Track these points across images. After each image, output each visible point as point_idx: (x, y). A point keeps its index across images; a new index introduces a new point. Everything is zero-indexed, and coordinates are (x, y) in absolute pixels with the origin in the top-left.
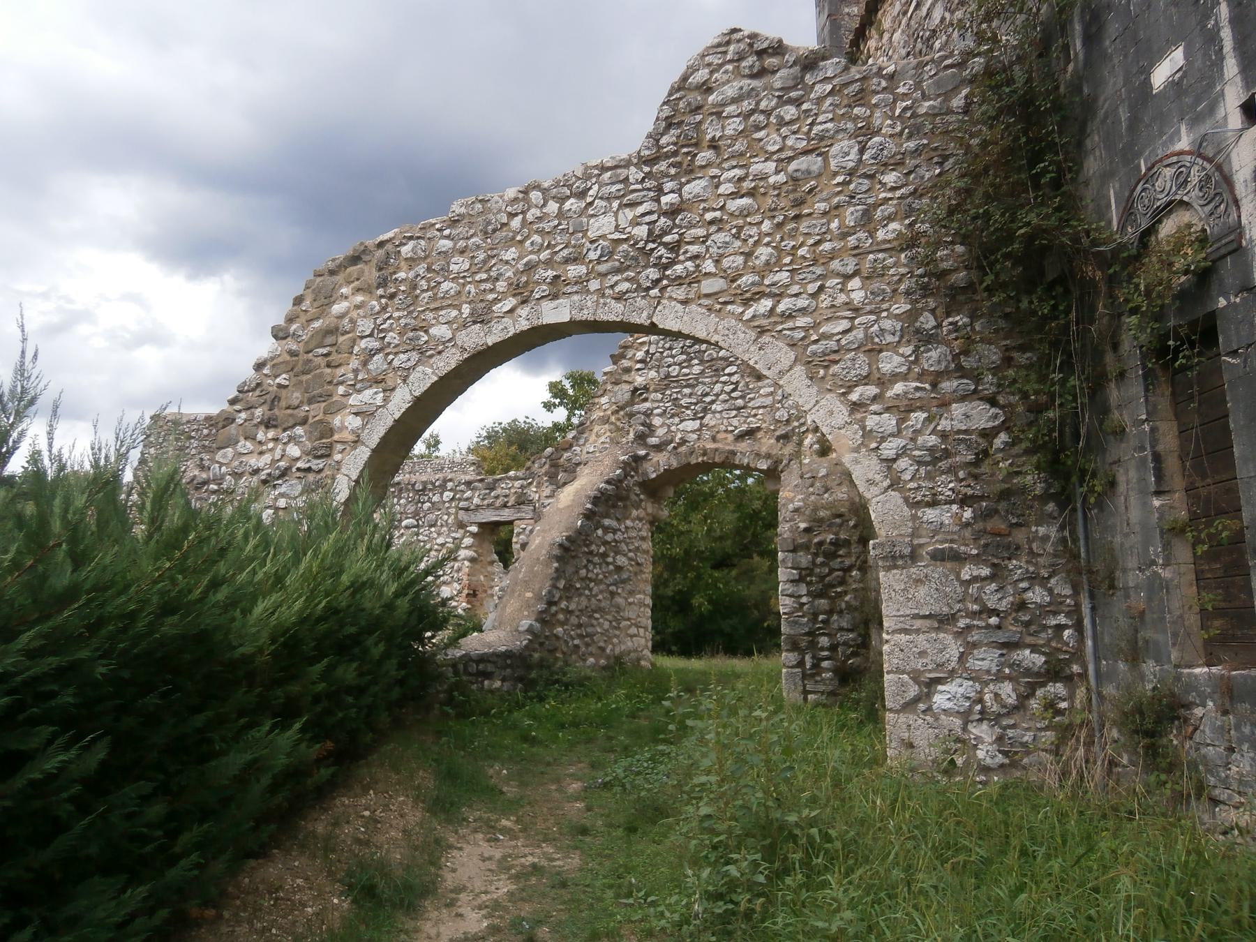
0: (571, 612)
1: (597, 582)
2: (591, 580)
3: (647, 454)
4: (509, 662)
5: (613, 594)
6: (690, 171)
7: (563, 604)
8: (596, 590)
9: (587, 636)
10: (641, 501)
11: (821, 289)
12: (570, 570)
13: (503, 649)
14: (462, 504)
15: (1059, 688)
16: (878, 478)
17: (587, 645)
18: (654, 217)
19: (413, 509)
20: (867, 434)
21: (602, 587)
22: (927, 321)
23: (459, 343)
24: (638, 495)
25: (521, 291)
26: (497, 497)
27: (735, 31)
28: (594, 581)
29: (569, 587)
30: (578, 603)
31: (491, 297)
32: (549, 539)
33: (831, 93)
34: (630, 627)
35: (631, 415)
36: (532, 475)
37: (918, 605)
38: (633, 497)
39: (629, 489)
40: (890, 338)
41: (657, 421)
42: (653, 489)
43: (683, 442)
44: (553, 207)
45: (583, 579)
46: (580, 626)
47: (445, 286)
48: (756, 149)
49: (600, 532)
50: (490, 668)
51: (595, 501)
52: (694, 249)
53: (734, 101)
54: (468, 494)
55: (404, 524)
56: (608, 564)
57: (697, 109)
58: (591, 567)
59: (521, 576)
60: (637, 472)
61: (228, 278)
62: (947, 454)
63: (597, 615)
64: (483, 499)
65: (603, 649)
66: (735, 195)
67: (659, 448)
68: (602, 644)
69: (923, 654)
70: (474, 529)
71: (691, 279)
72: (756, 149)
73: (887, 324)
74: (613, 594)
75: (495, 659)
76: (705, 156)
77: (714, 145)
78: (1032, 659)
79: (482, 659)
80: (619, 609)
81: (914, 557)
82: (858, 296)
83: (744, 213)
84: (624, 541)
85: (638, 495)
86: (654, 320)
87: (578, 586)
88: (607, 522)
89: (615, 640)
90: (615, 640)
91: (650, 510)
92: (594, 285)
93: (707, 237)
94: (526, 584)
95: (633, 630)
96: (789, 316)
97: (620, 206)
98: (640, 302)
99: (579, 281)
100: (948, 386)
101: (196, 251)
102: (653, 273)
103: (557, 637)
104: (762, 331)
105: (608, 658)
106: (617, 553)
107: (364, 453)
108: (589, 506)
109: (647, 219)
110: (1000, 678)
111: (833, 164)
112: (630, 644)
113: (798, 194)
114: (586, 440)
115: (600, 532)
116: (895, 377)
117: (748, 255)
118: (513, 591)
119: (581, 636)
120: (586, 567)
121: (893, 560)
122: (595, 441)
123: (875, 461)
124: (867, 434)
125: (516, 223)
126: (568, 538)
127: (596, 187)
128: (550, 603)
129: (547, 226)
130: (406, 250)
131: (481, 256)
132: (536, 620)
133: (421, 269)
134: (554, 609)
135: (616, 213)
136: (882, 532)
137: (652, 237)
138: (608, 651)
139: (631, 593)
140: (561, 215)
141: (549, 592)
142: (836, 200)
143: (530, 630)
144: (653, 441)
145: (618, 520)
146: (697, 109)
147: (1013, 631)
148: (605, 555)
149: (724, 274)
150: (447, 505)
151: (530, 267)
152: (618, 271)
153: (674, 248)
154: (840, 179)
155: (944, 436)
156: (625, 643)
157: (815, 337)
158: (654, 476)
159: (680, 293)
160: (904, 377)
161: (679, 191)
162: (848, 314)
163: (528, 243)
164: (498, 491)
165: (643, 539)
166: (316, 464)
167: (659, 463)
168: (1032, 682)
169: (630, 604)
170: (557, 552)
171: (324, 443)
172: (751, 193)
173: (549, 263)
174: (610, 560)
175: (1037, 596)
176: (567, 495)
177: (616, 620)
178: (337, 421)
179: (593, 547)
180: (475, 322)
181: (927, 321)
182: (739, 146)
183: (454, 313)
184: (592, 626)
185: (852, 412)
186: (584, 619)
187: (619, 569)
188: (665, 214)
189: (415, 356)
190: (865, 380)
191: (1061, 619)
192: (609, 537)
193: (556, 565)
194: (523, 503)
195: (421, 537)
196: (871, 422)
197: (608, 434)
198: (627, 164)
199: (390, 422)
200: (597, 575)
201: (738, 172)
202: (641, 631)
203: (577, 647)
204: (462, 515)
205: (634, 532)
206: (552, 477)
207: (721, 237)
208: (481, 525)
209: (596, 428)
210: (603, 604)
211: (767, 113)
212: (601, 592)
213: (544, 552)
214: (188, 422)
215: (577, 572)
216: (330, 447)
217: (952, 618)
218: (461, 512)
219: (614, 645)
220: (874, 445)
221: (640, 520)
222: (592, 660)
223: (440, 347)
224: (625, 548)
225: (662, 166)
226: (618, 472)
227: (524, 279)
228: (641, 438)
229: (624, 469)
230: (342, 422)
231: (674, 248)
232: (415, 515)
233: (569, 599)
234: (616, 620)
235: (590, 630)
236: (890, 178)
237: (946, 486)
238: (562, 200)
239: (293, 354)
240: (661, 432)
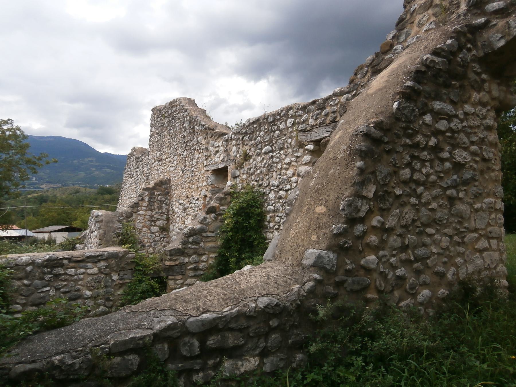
0: (390, 231)
1: (427, 184)
2: (418, 183)
3: (487, 22)
4: (274, 323)
5: (452, 200)
8: (426, 196)
9: (416, 260)
10: (484, 81)
12: (383, 169)
13: (264, 301)
14: (301, 127)
17: (418, 272)
19: (268, 137)
21: (436, 191)
24: (478, 74)
26: (327, 115)
28: (423, 184)
30: (400, 217)
32: (351, 130)
34: (478, 239)
38: (472, 76)
39: (465, 65)
45: (405, 183)
46: (404, 248)
49: (428, 118)
50: (231, 340)
54: (305, 117)
55: (263, 151)
56: (443, 161)
58: (417, 165)
59: (312, 184)
60: (475, 46)
61: (272, 78)
64: (316, 119)
65: (442, 275)
68: (440, 268)
70: (311, 147)
74: (452, 200)
75: (244, 323)
80: (461, 218)
84: (463, 130)
85: (478, 74)
87: (399, 192)
88: (437, 105)
89: (459, 260)
90: (459, 260)
91: (495, 93)
95: (483, 243)
101: (257, 70)
103: (368, 270)
105: (450, 285)
106: (454, 146)
108: (409, 83)
112: (479, 261)
114: (408, 35)
115: (428, 118)
118: (301, 206)
119: (407, 262)
120: (409, 165)
122: (418, 32)
126: (378, 125)
132: (329, 248)
134: (359, 228)
138: (449, 276)
139: (478, 196)
141: (350, 205)
143: (318, 265)
145: (453, 103)
148: (437, 149)
150: (290, 130)
156: (472, 261)
158: (502, 43)
164: (328, 109)
165: (489, 128)
169: (477, 211)
170: (361, 145)
174: (445, 155)
177: (459, 233)
179: (419, 138)
184: (424, 245)
186: (411, 238)
187: (458, 167)
192: (442, 125)
193: (359, 163)
195: (274, 160)
197: (433, 19)
200: (428, 175)
202: (494, 242)
203: (401, 279)
204: (302, 137)
209: (418, 18)
210: (438, 215)
212: (435, 198)
213: (343, 147)
214: (164, 108)
215: (396, 173)
218: (301, 134)
219: (457, 267)
221: (484, 105)
222: (426, 292)
224: (465, 140)
226: (449, 42)
229: (457, 39)
232: (270, 142)
233: (384, 212)
234: (459, 233)
235: (420, 252)
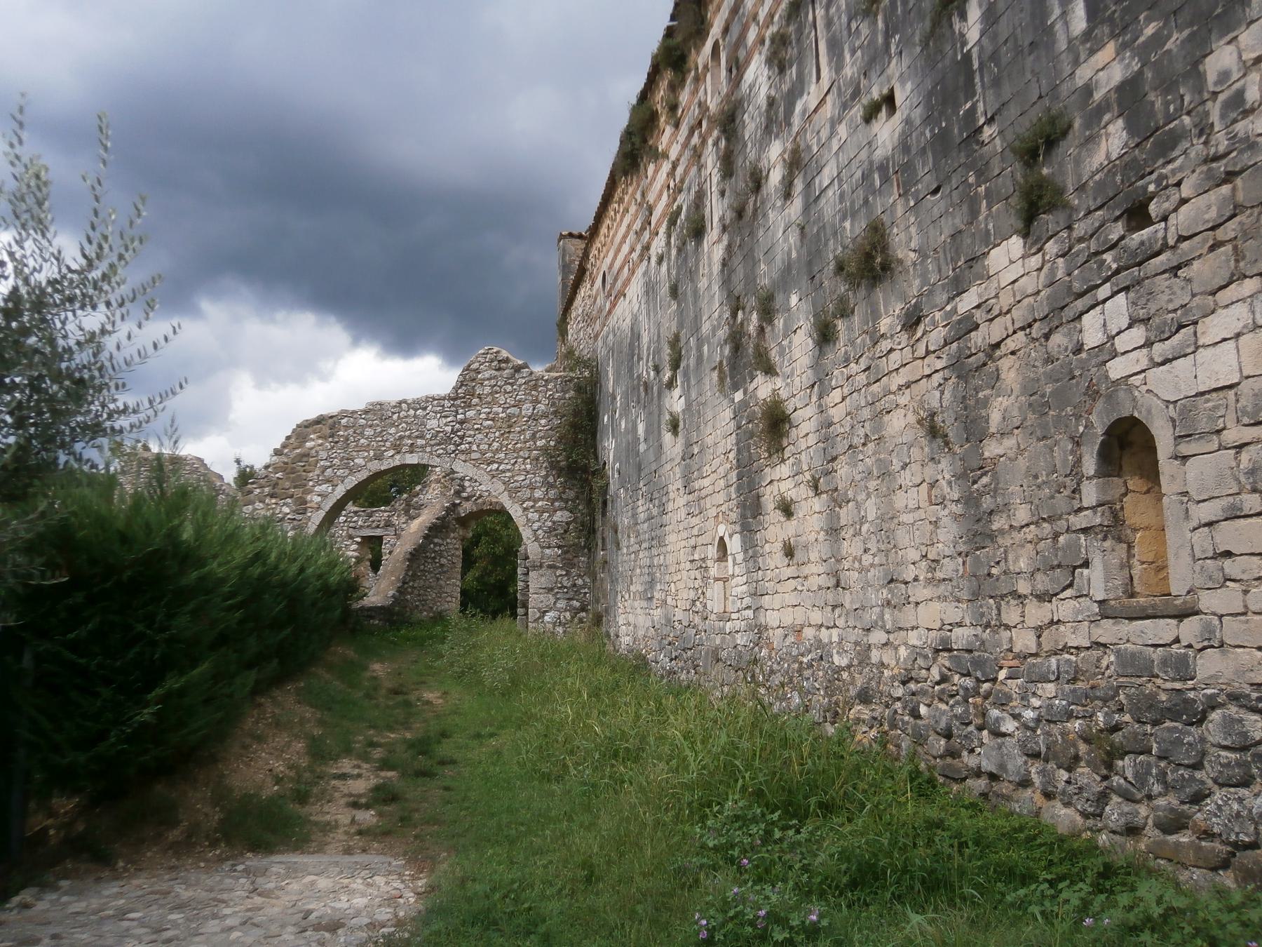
1: (430, 572)
6: (469, 406)
12: (415, 565)
15: (583, 614)
20: (528, 520)
22: (551, 479)
25: (397, 448)
29: (414, 575)
35: (453, 479)
36: (395, 510)
41: (467, 484)
42: (463, 522)
43: (481, 496)
44: (412, 412)
47: (362, 441)
48: (495, 402)
51: (430, 529)
52: (469, 439)
57: (474, 380)
66: (487, 419)
67: (467, 499)
70: (359, 540)
71: (468, 452)
72: (495, 402)
74: (438, 579)
76: (475, 401)
77: (479, 397)
78: (576, 604)
79: (370, 609)
80: (441, 587)
81: (541, 566)
82: (528, 466)
83: (490, 427)
92: (428, 449)
94: (392, 573)
100: (557, 504)
102: (452, 447)
104: (493, 477)
107: (322, 514)
110: (566, 610)
113: (510, 422)
116: (540, 499)
117: (490, 445)
124: (528, 520)
125: (395, 417)
128: (404, 583)
129: (409, 420)
130: (344, 421)
131: (379, 430)
133: (351, 431)
137: (453, 432)
139: (449, 579)
140: (415, 416)
143: (393, 596)
144: (465, 495)
146: (474, 380)
147: (571, 594)
148: (434, 558)
149: (480, 451)
151: (401, 438)
152: (439, 444)
153: (462, 438)
155: (554, 523)
159: (463, 457)
160: (542, 500)
166: (300, 517)
167: (467, 507)
168: (575, 611)
171: (302, 507)
172: (493, 420)
173: (409, 437)
175: (580, 582)
176: (415, 525)
178: (309, 497)
181: (551, 479)
182: (489, 399)
187: (442, 566)
189: (347, 471)
190: (529, 499)
192: (437, 548)
196: (530, 515)
198: (444, 399)
205: (453, 545)
206: (407, 512)
207: (480, 436)
211: (500, 387)
216: (305, 509)
217: (552, 589)
223: (360, 468)
225: (458, 402)
228: (458, 493)
231: (462, 438)
236: (543, 422)
237: (554, 541)
238: (416, 410)
239: (286, 463)
240: (469, 490)
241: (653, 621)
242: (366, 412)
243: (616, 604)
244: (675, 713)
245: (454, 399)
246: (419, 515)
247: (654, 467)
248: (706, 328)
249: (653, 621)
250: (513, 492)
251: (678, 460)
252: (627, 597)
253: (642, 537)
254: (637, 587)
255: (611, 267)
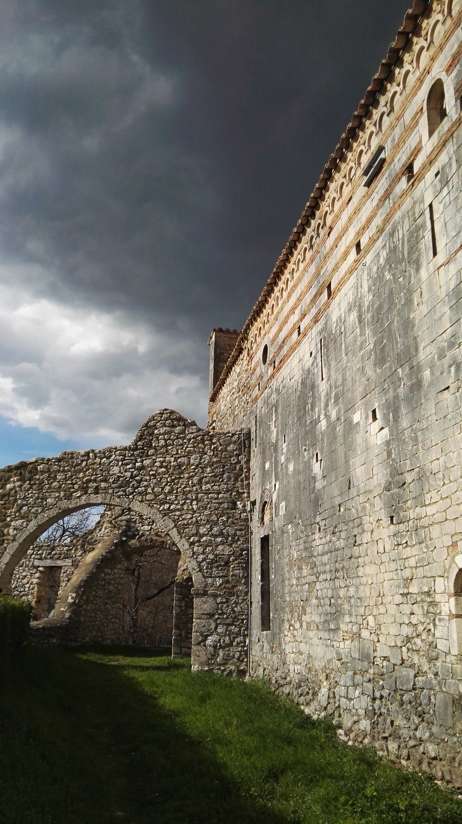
0: (87, 611)
2: (97, 596)
5: (106, 603)
7: (85, 607)
9: (93, 621)
11: (185, 503)
16: (196, 568)
18: (133, 470)
20: (194, 553)
23: (59, 506)
27: (166, 410)
31: (72, 490)
33: (193, 438)
34: (112, 618)
37: (204, 610)
40: (203, 522)
43: (143, 535)
49: (103, 575)
52: (146, 483)
53: (162, 434)
56: (105, 589)
58: (98, 591)
62: (217, 561)
63: (98, 613)
66: (161, 467)
69: (204, 626)
73: (203, 518)
74: (106, 603)
76: (151, 452)
86: (130, 506)
92: (110, 491)
93: (150, 480)
96: (173, 511)
97: (122, 464)
98: (126, 500)
99: (105, 488)
104: (165, 515)
109: (131, 470)
111: (192, 461)
117: (163, 489)
120: (95, 590)
121: (198, 595)
123: (195, 562)
127: (114, 456)
129: (95, 466)
131: (69, 474)
134: (81, 609)
135: (120, 467)
136: (196, 585)
137: (132, 477)
139: (114, 603)
142: (191, 474)
148: (104, 585)
153: (140, 482)
154: (193, 467)
155: (216, 556)
157: (181, 519)
161: (142, 462)
162: (191, 512)
163: (87, 472)
169: (113, 608)
173: (95, 481)
174: (106, 587)
180: (65, 499)
183: (57, 494)
185: (190, 546)
187: (110, 592)
188: (137, 469)
190: (196, 535)
191: (244, 617)
192: (107, 577)
194: (67, 558)
196: (195, 549)
198: (125, 449)
199: (28, 533)
201: (161, 459)
208: (45, 567)
220: (195, 557)
227: (85, 485)
230: (8, 531)
233: (87, 605)
241: (338, 653)
242: (59, 460)
243: (281, 631)
244: (242, 703)
245: (134, 450)
246: (94, 549)
247: (337, 501)
248: (425, 353)
249: (338, 653)
250: (181, 530)
251: (379, 490)
252: (297, 626)
253: (320, 569)
254: (313, 616)
255: (276, 336)
